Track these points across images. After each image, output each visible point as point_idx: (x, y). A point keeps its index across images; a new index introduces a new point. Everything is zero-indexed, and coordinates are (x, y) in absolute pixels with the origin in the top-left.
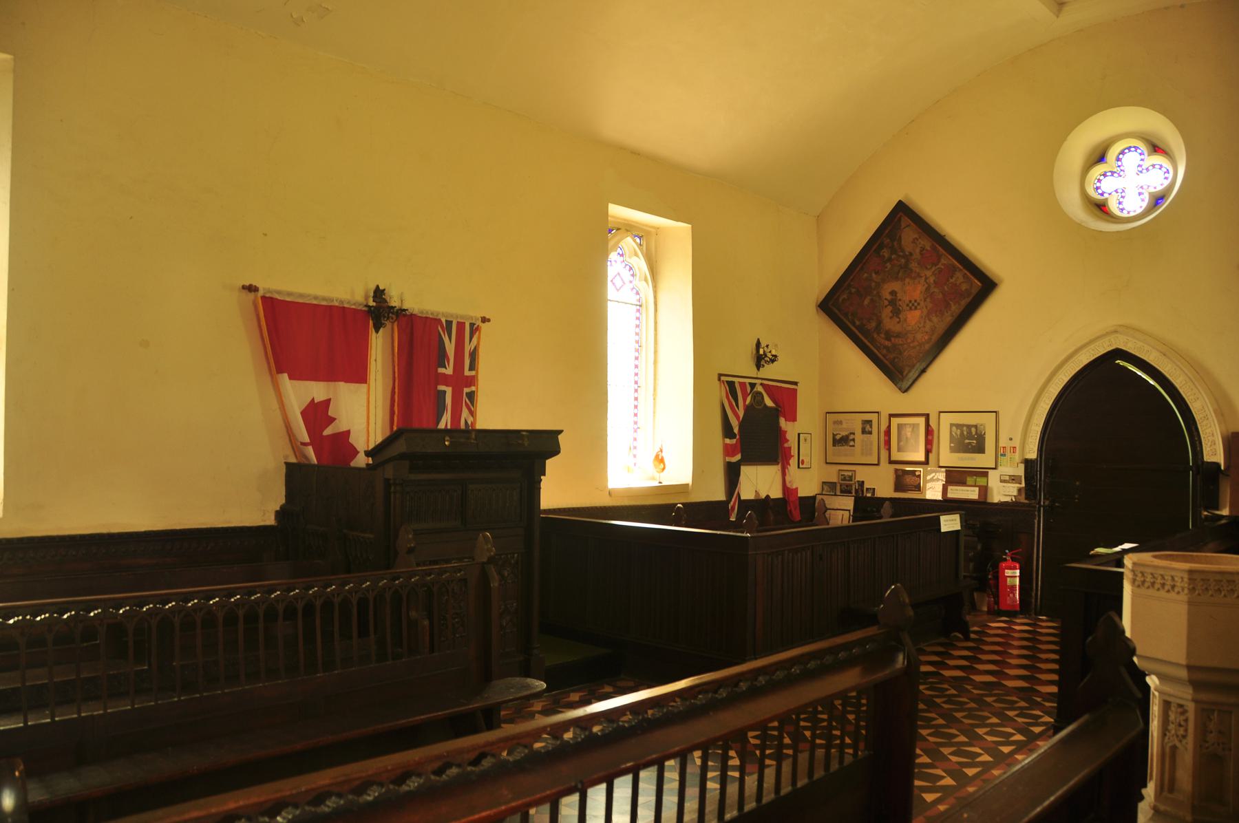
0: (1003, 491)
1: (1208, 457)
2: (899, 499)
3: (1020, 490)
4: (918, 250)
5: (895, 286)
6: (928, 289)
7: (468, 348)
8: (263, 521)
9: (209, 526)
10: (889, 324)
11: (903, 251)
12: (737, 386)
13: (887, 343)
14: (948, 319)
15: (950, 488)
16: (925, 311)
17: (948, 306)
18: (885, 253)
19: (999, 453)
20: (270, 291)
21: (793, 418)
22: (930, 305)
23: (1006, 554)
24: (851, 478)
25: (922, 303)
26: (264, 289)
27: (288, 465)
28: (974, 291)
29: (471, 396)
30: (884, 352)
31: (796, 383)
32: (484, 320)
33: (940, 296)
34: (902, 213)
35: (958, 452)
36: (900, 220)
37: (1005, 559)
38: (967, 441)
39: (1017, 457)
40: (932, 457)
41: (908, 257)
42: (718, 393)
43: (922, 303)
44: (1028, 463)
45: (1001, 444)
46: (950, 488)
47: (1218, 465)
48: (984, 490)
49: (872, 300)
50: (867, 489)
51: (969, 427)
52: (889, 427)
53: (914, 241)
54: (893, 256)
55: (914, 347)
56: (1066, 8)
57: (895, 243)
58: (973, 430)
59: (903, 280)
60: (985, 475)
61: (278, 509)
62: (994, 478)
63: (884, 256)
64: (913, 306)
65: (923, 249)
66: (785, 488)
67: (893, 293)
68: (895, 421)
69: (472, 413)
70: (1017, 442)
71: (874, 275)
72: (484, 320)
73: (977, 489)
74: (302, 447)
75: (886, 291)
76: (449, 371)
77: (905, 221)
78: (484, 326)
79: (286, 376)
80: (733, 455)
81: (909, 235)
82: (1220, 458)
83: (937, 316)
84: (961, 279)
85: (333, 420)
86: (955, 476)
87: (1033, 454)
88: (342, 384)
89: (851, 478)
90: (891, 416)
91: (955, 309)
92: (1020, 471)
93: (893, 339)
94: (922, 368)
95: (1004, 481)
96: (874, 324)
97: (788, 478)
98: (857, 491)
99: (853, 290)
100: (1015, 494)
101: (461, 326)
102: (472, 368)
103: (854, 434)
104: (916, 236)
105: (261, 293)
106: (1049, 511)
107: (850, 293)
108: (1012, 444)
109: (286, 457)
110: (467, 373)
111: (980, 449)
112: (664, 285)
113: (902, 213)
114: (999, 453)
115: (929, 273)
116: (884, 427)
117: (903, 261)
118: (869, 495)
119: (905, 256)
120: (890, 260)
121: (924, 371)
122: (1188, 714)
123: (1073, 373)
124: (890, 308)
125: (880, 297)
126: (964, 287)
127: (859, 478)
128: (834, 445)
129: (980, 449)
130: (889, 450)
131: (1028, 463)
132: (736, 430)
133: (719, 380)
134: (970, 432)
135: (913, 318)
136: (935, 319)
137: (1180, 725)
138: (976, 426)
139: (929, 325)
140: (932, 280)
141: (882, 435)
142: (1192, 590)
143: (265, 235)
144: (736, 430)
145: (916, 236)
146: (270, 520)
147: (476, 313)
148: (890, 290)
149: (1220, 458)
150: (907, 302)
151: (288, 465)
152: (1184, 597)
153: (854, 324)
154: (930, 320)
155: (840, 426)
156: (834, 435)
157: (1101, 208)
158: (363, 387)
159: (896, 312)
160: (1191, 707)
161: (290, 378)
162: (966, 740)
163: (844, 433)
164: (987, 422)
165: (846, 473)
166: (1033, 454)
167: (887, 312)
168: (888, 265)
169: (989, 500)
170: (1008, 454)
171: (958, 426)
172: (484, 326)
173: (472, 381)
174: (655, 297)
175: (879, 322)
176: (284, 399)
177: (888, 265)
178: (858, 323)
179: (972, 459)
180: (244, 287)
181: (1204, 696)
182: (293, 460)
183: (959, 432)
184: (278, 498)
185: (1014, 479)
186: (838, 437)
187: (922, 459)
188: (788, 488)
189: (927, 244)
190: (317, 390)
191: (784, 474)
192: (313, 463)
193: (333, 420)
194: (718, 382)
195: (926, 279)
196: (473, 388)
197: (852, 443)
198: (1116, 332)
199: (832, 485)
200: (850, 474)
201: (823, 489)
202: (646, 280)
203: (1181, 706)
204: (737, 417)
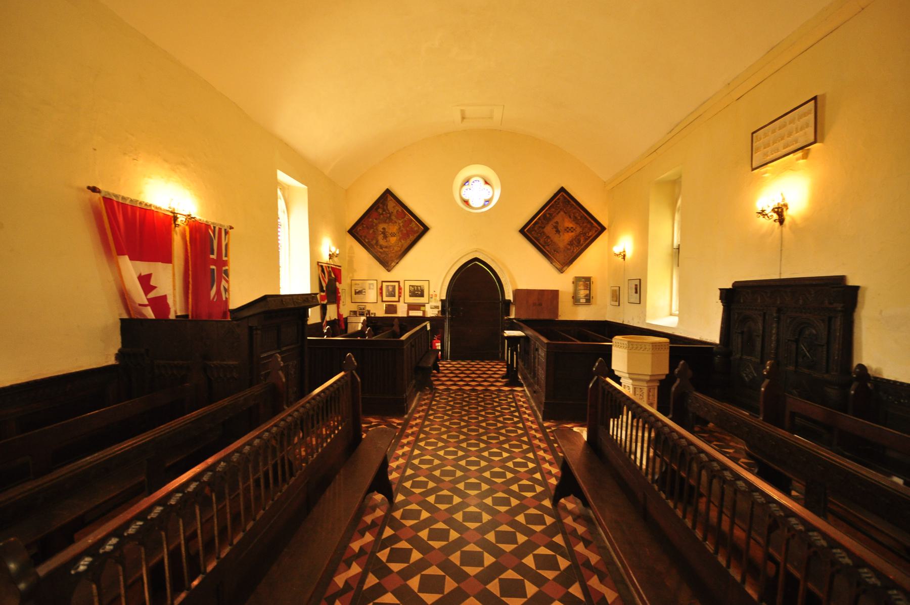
0: (431, 312)
1: (507, 298)
2: (387, 317)
3: (438, 312)
4: (395, 211)
5: (385, 226)
6: (400, 228)
7: (224, 244)
8: (106, 362)
9: (65, 373)
10: (382, 242)
11: (389, 211)
12: (324, 267)
13: (381, 250)
14: (409, 242)
15: (410, 312)
16: (398, 237)
17: (408, 236)
18: (380, 211)
19: (430, 297)
20: (109, 194)
21: (340, 283)
22: (401, 235)
23: (435, 337)
24: (364, 309)
25: (397, 234)
26: (105, 192)
27: (122, 320)
28: (420, 231)
29: (226, 272)
30: (380, 254)
31: (340, 266)
32: (231, 228)
33: (405, 232)
34: (388, 193)
35: (413, 296)
36: (387, 197)
37: (435, 339)
38: (416, 292)
39: (438, 298)
40: (402, 299)
41: (391, 214)
42: (318, 271)
43: (397, 234)
44: (442, 301)
45: (431, 293)
46: (410, 312)
47: (510, 301)
48: (424, 312)
49: (374, 231)
50: (372, 313)
51: (417, 286)
52: (382, 287)
53: (394, 207)
54: (384, 213)
55: (393, 253)
56: (465, 120)
57: (385, 207)
58: (419, 288)
59: (388, 223)
60: (424, 306)
61: (116, 352)
62: (428, 308)
63: (379, 212)
64: (393, 235)
65: (398, 211)
66: (339, 315)
67: (384, 229)
68: (384, 284)
69: (227, 282)
70: (438, 293)
71: (375, 220)
72: (231, 228)
73: (422, 312)
74: (141, 307)
75: (381, 227)
76: (214, 257)
77: (390, 197)
78: (231, 231)
79: (127, 257)
80: (324, 301)
81: (391, 204)
82: (511, 298)
83: (404, 240)
84: (414, 226)
85: (154, 288)
86: (411, 307)
87: (444, 298)
88: (160, 264)
89: (364, 309)
90: (383, 282)
91: (412, 238)
92: (439, 304)
93: (384, 249)
94: (397, 262)
95: (432, 308)
96: (374, 242)
97: (340, 310)
98: (367, 314)
99: (365, 226)
100: (437, 313)
101: (220, 230)
102: (226, 256)
103: (364, 289)
104: (395, 205)
105: (103, 194)
106: (451, 320)
107: (363, 227)
108: (435, 293)
109: (120, 315)
110: (224, 259)
111: (422, 295)
112: (293, 215)
113: (388, 193)
114: (430, 297)
115: (400, 222)
116: (379, 286)
117: (388, 215)
118: (373, 316)
119: (389, 213)
120: (382, 214)
121: (397, 263)
122: (644, 391)
123: (460, 266)
124: (382, 235)
125: (377, 229)
126: (416, 229)
127: (367, 308)
128: (355, 294)
129: (422, 295)
130: (382, 296)
131: (442, 301)
132: (325, 289)
133: (318, 264)
134: (418, 289)
135: (393, 240)
136: (403, 241)
137: (641, 395)
138: (420, 286)
139: (400, 244)
140: (401, 225)
141: (379, 290)
142: (653, 349)
143: (95, 150)
144: (325, 289)
145: (395, 205)
146: (112, 361)
147: (226, 224)
148: (382, 227)
149: (511, 298)
150: (390, 232)
151: (122, 320)
152: (650, 352)
153: (365, 241)
154: (401, 242)
155: (358, 286)
156: (355, 290)
157: (466, 202)
158: (170, 265)
159: (385, 237)
160: (631, 387)
161: (131, 259)
162: (433, 412)
163: (360, 289)
164: (425, 285)
165: (361, 307)
166: (444, 298)
167: (380, 237)
168: (382, 216)
169: (426, 316)
170: (433, 297)
171: (412, 286)
172: (231, 231)
173: (225, 263)
174: (289, 222)
175: (377, 241)
176: (123, 273)
177: (382, 216)
178: (367, 240)
179: (418, 299)
180: (89, 188)
181: (637, 383)
182: (125, 316)
183: (413, 289)
184: (116, 344)
185: (437, 307)
186: (357, 291)
187: (397, 300)
188: (340, 315)
189: (400, 208)
190: (144, 267)
191: (338, 307)
192: (149, 318)
193: (154, 288)
194: (317, 266)
195: (399, 224)
196: (227, 268)
197: (364, 293)
198: (476, 251)
199: (355, 313)
200: (363, 307)
201: (350, 314)
202: (284, 212)
203: (628, 386)
204: (325, 282)
